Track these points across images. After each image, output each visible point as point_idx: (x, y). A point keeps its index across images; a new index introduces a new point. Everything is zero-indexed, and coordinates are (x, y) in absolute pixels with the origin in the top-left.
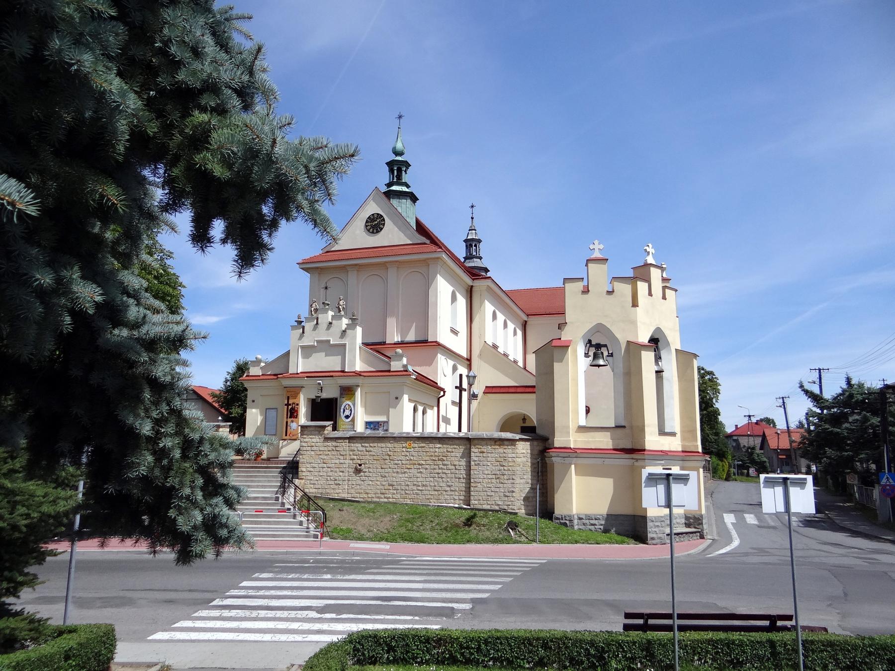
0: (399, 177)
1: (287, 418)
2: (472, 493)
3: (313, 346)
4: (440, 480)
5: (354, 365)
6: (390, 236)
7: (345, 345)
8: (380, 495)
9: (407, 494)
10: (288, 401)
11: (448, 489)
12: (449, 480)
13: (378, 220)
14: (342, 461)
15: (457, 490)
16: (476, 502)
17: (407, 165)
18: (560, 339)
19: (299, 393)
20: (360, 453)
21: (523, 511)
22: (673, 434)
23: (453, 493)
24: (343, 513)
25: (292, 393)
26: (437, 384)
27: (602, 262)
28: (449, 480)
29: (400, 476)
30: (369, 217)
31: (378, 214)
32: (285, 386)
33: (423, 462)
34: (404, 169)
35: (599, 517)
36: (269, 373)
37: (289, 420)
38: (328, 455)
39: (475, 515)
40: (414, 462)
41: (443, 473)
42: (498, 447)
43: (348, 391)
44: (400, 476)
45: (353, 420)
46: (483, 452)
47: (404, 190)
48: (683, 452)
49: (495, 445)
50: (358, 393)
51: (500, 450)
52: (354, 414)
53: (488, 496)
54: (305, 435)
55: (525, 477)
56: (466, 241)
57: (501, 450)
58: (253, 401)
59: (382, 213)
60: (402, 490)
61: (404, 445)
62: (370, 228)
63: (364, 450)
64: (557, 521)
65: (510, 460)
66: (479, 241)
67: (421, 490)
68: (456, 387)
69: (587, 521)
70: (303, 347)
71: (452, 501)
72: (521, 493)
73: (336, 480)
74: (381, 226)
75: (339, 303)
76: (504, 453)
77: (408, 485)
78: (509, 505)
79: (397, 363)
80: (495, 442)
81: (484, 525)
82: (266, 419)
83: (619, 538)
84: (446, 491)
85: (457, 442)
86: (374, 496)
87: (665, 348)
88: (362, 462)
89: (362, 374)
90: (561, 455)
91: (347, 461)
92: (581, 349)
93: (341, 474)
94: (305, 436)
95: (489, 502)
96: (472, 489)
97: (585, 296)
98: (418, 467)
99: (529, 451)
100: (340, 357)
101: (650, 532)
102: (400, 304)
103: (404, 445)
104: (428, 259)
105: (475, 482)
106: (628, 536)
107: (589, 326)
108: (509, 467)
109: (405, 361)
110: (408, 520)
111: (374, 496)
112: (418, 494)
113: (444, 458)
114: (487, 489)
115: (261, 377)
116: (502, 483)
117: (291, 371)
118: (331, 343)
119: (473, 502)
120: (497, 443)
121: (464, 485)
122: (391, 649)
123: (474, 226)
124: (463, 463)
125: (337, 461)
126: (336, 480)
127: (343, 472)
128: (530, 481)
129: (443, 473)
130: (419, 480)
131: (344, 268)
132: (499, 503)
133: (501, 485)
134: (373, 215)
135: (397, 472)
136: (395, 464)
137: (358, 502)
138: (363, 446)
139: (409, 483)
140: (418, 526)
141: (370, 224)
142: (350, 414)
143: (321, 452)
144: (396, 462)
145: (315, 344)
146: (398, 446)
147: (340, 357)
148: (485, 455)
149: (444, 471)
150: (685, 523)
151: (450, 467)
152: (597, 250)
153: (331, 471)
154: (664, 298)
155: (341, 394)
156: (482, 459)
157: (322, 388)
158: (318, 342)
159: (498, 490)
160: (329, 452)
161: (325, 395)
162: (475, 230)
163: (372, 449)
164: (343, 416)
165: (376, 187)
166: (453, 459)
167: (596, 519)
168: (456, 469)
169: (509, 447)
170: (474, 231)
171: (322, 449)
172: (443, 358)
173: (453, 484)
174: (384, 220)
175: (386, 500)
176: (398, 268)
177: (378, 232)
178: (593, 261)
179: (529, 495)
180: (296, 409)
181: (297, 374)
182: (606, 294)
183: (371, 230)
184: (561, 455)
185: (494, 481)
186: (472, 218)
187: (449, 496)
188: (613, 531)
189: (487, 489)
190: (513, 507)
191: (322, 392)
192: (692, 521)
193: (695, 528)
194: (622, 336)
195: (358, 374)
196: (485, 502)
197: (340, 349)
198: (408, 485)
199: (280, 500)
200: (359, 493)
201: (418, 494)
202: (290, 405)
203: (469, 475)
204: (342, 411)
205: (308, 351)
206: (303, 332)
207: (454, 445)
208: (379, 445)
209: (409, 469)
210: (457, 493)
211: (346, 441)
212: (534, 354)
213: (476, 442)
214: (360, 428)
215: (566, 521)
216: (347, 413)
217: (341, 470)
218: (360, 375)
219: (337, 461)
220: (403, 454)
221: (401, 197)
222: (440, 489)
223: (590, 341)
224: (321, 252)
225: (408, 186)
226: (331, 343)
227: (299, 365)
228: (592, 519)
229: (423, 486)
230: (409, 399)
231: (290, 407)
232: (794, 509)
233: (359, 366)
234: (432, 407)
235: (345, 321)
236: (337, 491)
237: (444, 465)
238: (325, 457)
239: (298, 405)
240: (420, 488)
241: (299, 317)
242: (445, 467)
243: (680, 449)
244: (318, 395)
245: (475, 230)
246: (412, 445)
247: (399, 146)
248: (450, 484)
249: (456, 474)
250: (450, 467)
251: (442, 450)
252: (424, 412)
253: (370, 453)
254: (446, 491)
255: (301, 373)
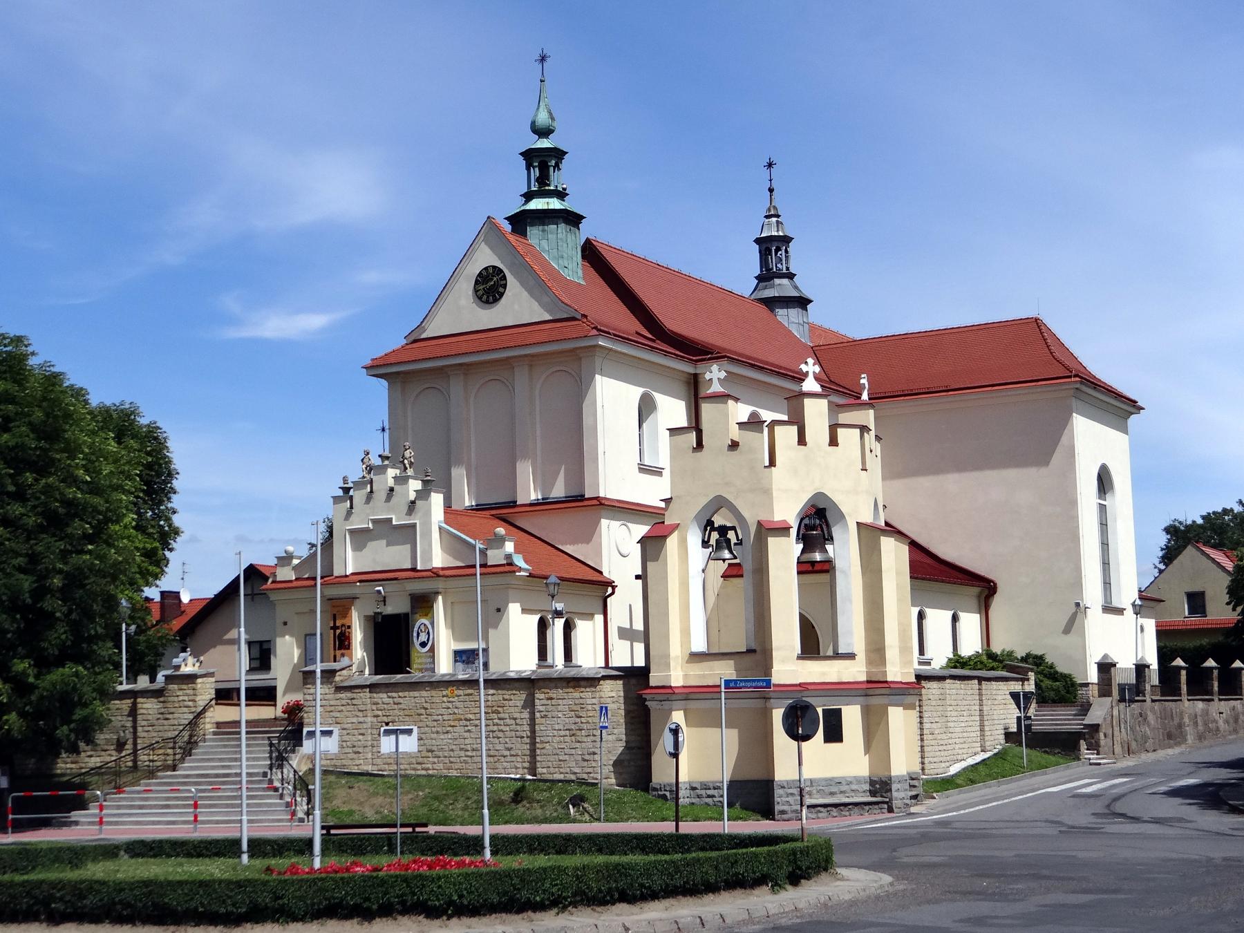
0: (543, 179)
1: (335, 649)
2: (538, 758)
3: (366, 530)
4: (496, 741)
5: (431, 559)
6: (516, 307)
7: (414, 526)
8: (416, 766)
9: (452, 763)
10: (335, 623)
11: (507, 753)
12: (507, 740)
13: (495, 279)
14: (361, 720)
15: (520, 754)
16: (545, 770)
17: (558, 154)
18: (663, 522)
19: (351, 608)
20: (385, 706)
21: (613, 781)
22: (851, 656)
23: (513, 759)
24: (351, 791)
25: (338, 609)
26: (601, 573)
27: (721, 399)
28: (507, 740)
29: (442, 737)
30: (480, 274)
31: (494, 267)
32: (328, 597)
33: (471, 716)
34: (553, 163)
35: (718, 784)
36: (306, 576)
37: (338, 653)
38: (342, 711)
39: (523, 787)
40: (459, 716)
41: (499, 731)
42: (571, 690)
43: (423, 603)
44: (442, 737)
45: (432, 650)
46: (551, 699)
47: (551, 207)
48: (868, 682)
49: (568, 687)
50: (439, 605)
51: (575, 694)
52: (433, 638)
53: (560, 761)
54: (309, 684)
55: (616, 731)
56: (758, 241)
57: (577, 695)
58: (285, 624)
59: (501, 266)
60: (445, 757)
61: (444, 693)
62: (483, 294)
63: (392, 702)
64: (654, 793)
65: (590, 707)
66: (786, 240)
67: (471, 757)
68: (638, 577)
69: (703, 792)
70: (352, 532)
71: (513, 770)
72: (610, 755)
73: (354, 747)
74: (501, 290)
75: (403, 456)
76: (581, 698)
77: (452, 750)
78: (590, 773)
79: (496, 551)
80: (568, 682)
81: (538, 801)
82: (306, 651)
83: (743, 814)
84: (504, 757)
85: (517, 685)
86: (407, 767)
87: (838, 523)
88: (390, 719)
89: (441, 573)
90: (657, 697)
91: (369, 719)
92: (694, 537)
93: (361, 737)
94: (308, 686)
95: (561, 770)
96: (538, 752)
97: (698, 454)
98: (465, 723)
99: (622, 694)
100: (408, 547)
101: (778, 803)
102: (538, 433)
103: (444, 693)
104: (577, 348)
105: (542, 742)
106: (754, 811)
107: (704, 501)
108: (589, 719)
109: (509, 547)
110: (436, 798)
111: (407, 767)
112: (466, 762)
113: (500, 709)
114: (558, 751)
115: (295, 584)
116: (579, 742)
117: (336, 574)
118: (394, 523)
119: (540, 770)
120: (571, 684)
121: (528, 746)
122: (152, 849)
123: (775, 207)
124: (526, 715)
125: (355, 720)
126: (354, 747)
127: (363, 734)
128: (624, 737)
129: (499, 731)
130: (467, 741)
131: (441, 370)
132: (576, 771)
133: (578, 745)
134: (486, 269)
135: (438, 732)
136: (434, 721)
137: (382, 776)
138: (389, 697)
139: (454, 747)
140: (445, 805)
141: (481, 287)
142: (428, 640)
143: (332, 708)
144: (435, 717)
145: (371, 526)
146: (437, 695)
147: (408, 547)
148: (554, 702)
149: (501, 728)
150: (870, 791)
151: (508, 721)
152: (715, 381)
153: (348, 734)
154: (833, 442)
155: (413, 607)
156: (550, 708)
157: (385, 597)
158: (375, 522)
159: (573, 751)
160: (343, 708)
161: (389, 610)
162: (778, 216)
163: (401, 700)
164: (417, 643)
165: (489, 217)
166: (512, 710)
167: (715, 788)
168: (516, 724)
169: (588, 690)
170: (774, 219)
171: (332, 703)
172: (615, 524)
173: (513, 746)
174: (504, 278)
175: (424, 772)
176: (531, 366)
177: (496, 300)
178: (707, 400)
179: (622, 758)
180: (347, 634)
181: (346, 576)
182: (728, 450)
183: (485, 297)
184: (657, 697)
185: (568, 739)
186: (771, 190)
187: (508, 764)
188: (737, 805)
189: (558, 751)
190: (595, 776)
191: (385, 605)
192: (878, 786)
193: (882, 796)
194: (752, 516)
195: (435, 574)
196: (557, 769)
197: (407, 534)
198: (452, 750)
199: (269, 777)
200: (388, 764)
201: (466, 762)
202: (338, 628)
203: (533, 731)
204: (415, 634)
205: (360, 537)
206: (351, 507)
207: (512, 690)
208: (412, 694)
209: (453, 726)
210: (519, 759)
211: (365, 690)
212: (639, 545)
213: (541, 683)
214: (444, 666)
215: (666, 793)
216: (423, 637)
217: (361, 731)
218: (438, 576)
219: (355, 720)
220: (444, 705)
221: (547, 221)
222: (497, 753)
223: (710, 523)
224: (405, 342)
225: (561, 195)
226: (394, 523)
227: (349, 561)
228: (710, 789)
229: (473, 750)
230: (522, 609)
231: (338, 631)
232: (400, 750)
233: (438, 558)
234: (589, 616)
235: (415, 485)
236: (357, 762)
237: (499, 719)
238: (338, 715)
239: (349, 627)
240: (469, 754)
241: (345, 480)
242: (502, 722)
243: (863, 678)
244: (379, 610)
245: (778, 216)
246: (456, 692)
247: (543, 118)
248: (509, 746)
249: (517, 731)
250: (508, 721)
251: (496, 698)
252: (568, 628)
253: (400, 706)
254: (504, 757)
255: (353, 574)
